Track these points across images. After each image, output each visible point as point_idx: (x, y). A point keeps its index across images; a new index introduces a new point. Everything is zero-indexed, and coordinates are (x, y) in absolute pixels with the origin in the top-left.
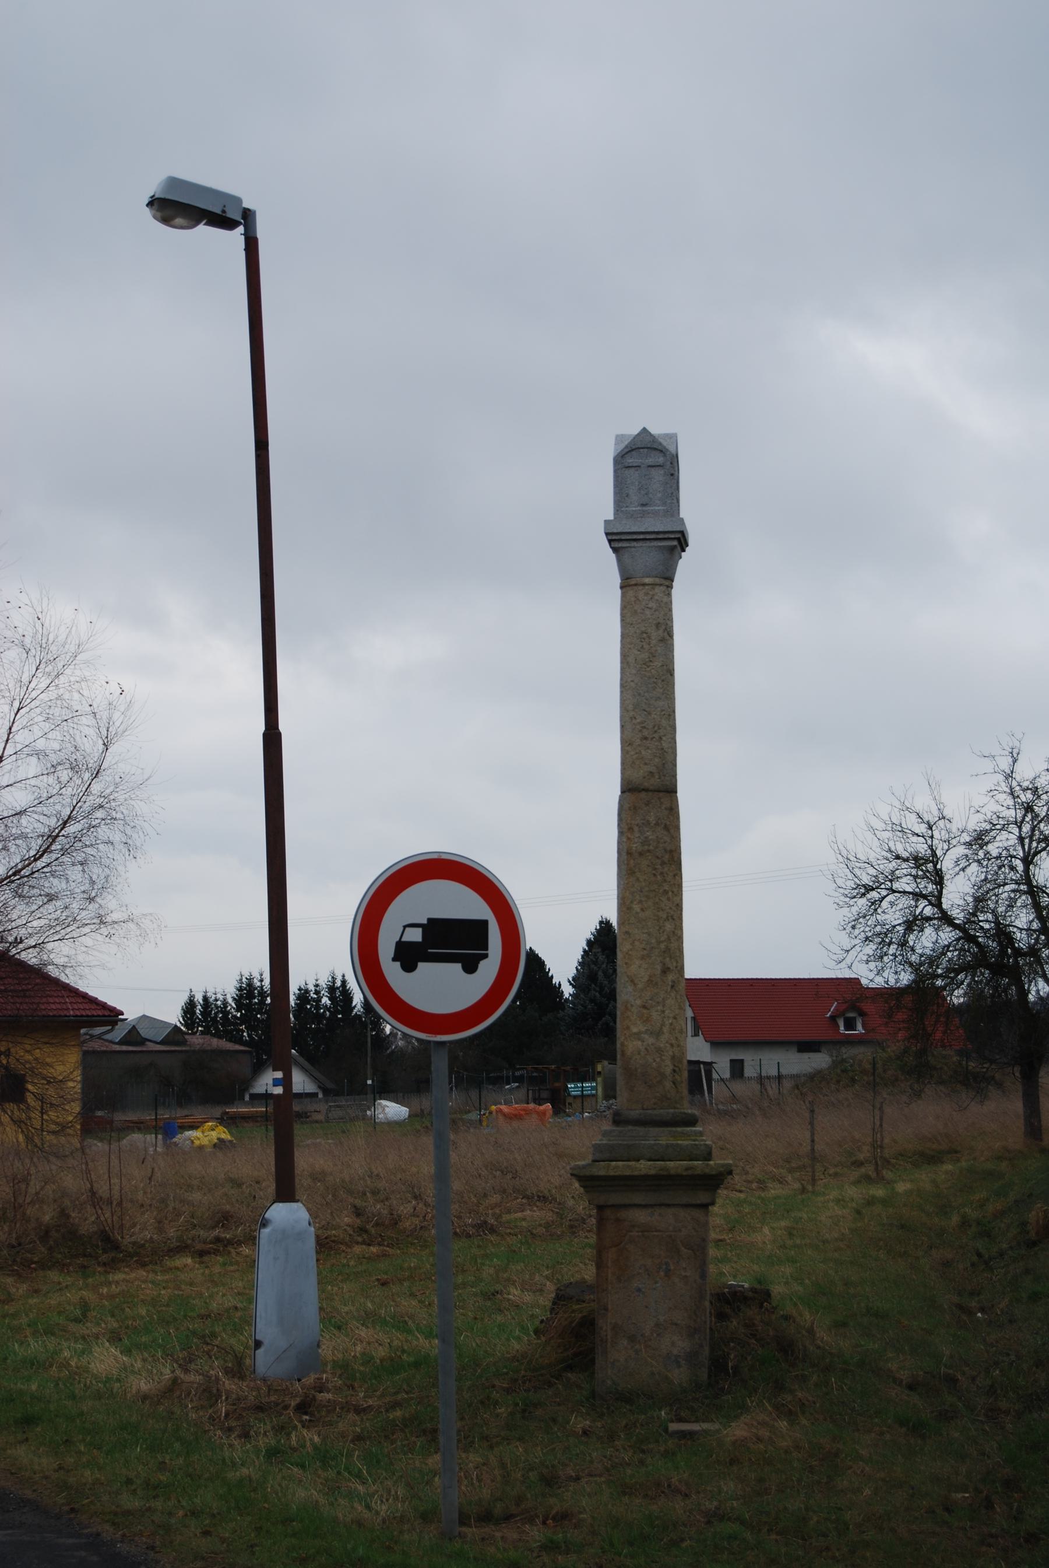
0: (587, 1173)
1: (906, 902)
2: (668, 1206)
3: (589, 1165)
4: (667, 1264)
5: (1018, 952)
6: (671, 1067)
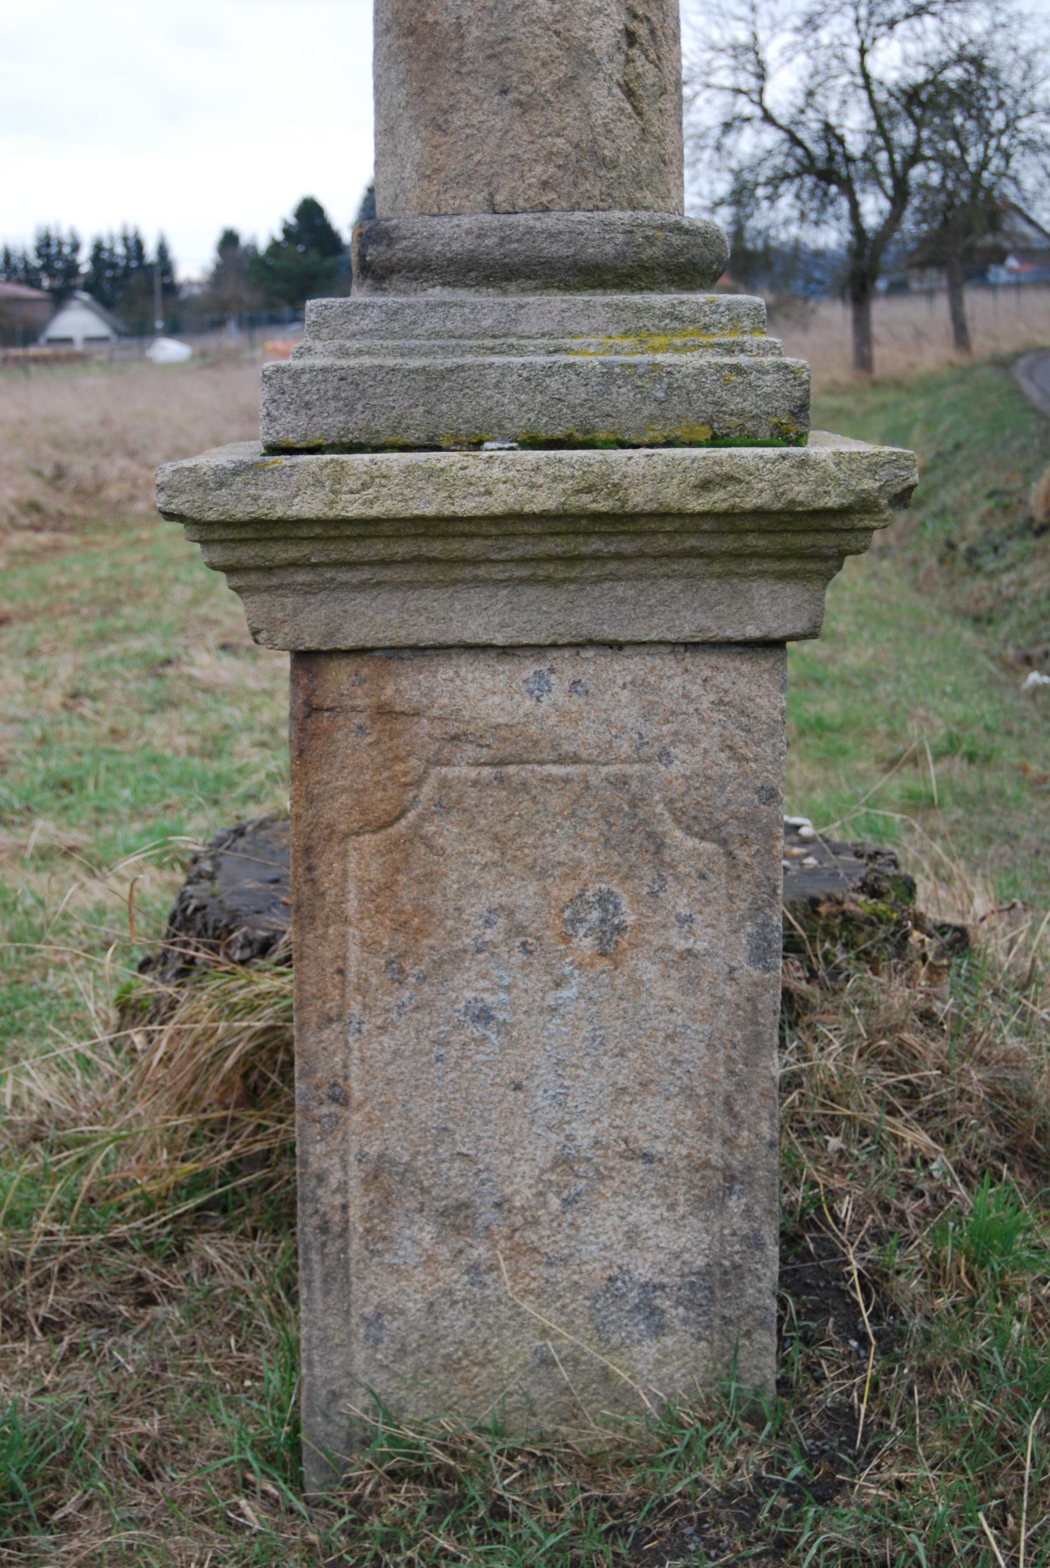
0: (237, 505)
1: (722, 99)
2: (616, 646)
3: (240, 469)
4: (604, 899)
5: (849, 159)
6: (619, 20)
